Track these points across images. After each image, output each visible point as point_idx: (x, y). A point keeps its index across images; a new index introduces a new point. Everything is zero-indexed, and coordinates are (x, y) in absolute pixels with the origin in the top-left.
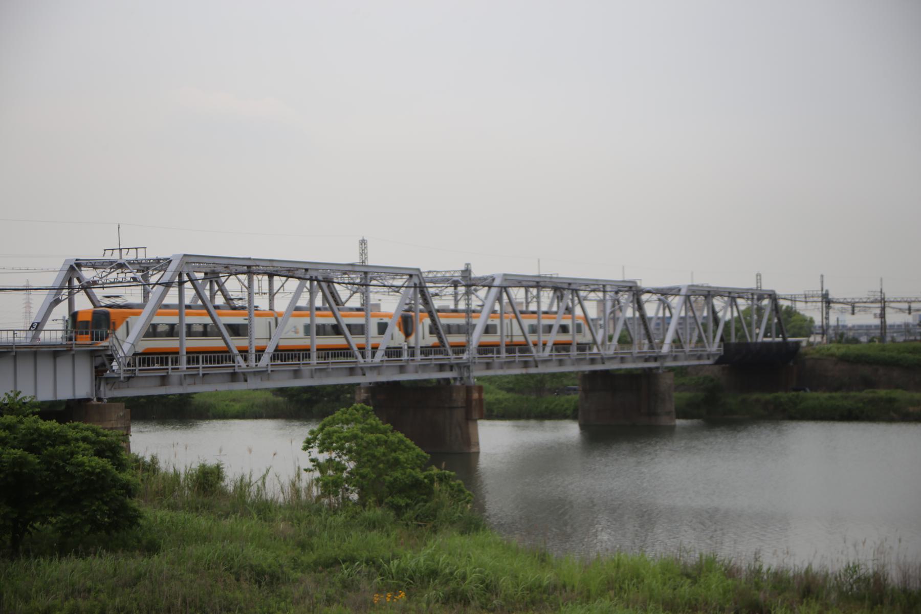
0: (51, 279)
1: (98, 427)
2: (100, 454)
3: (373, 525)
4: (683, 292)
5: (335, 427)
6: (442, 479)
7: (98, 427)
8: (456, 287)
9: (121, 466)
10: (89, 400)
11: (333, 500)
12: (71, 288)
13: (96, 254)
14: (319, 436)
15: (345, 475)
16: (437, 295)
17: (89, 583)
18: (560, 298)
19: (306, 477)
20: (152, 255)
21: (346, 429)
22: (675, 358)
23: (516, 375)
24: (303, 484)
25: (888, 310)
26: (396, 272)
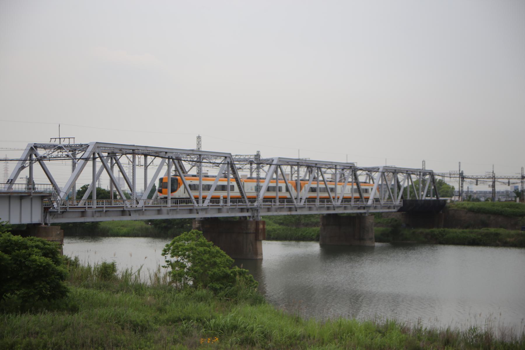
0: (20, 154)
1: (45, 240)
2: (45, 255)
3: (201, 299)
4: (381, 170)
5: (181, 243)
6: (241, 273)
7: (45, 240)
8: (251, 164)
9: (57, 262)
10: (40, 224)
11: (178, 284)
12: (31, 160)
13: (46, 141)
14: (172, 248)
15: (185, 270)
16: (240, 168)
17: (37, 329)
18: (311, 172)
19: (163, 271)
20: (78, 142)
21: (187, 244)
22: (375, 208)
23: (284, 215)
24: (162, 275)
25: (496, 183)
26: (217, 155)
